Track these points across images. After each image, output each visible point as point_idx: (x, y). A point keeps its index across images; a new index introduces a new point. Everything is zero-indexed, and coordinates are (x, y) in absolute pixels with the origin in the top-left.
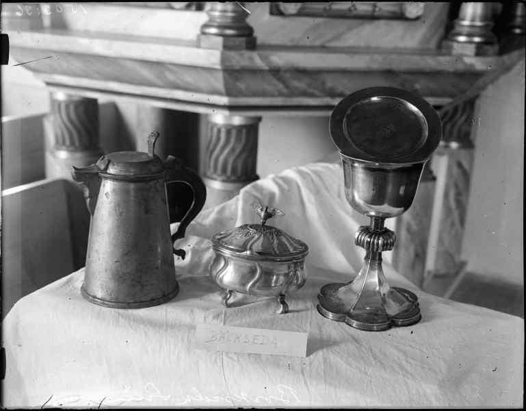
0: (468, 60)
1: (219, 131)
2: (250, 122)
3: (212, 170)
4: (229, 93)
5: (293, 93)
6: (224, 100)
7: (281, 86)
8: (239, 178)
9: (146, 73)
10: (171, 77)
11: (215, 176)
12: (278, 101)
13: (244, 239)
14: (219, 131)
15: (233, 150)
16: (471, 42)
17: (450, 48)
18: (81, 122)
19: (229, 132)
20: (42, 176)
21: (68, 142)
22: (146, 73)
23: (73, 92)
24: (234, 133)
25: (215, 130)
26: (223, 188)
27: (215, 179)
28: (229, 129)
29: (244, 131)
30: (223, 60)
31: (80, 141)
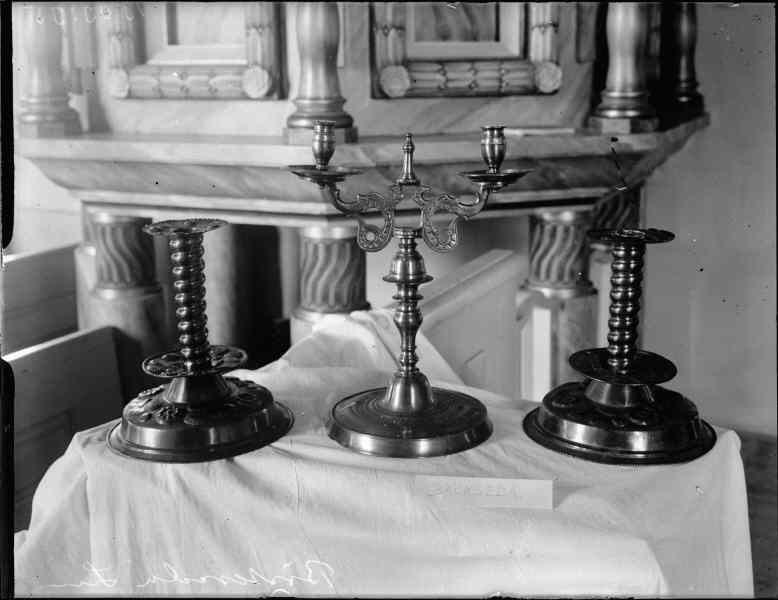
1: (316, 248)
3: (309, 298)
10: (250, 183)
11: (312, 307)
14: (316, 248)
15: (335, 271)
19: (328, 249)
20: (75, 328)
22: (221, 182)
24: (335, 249)
27: (313, 311)
31: (133, 275)
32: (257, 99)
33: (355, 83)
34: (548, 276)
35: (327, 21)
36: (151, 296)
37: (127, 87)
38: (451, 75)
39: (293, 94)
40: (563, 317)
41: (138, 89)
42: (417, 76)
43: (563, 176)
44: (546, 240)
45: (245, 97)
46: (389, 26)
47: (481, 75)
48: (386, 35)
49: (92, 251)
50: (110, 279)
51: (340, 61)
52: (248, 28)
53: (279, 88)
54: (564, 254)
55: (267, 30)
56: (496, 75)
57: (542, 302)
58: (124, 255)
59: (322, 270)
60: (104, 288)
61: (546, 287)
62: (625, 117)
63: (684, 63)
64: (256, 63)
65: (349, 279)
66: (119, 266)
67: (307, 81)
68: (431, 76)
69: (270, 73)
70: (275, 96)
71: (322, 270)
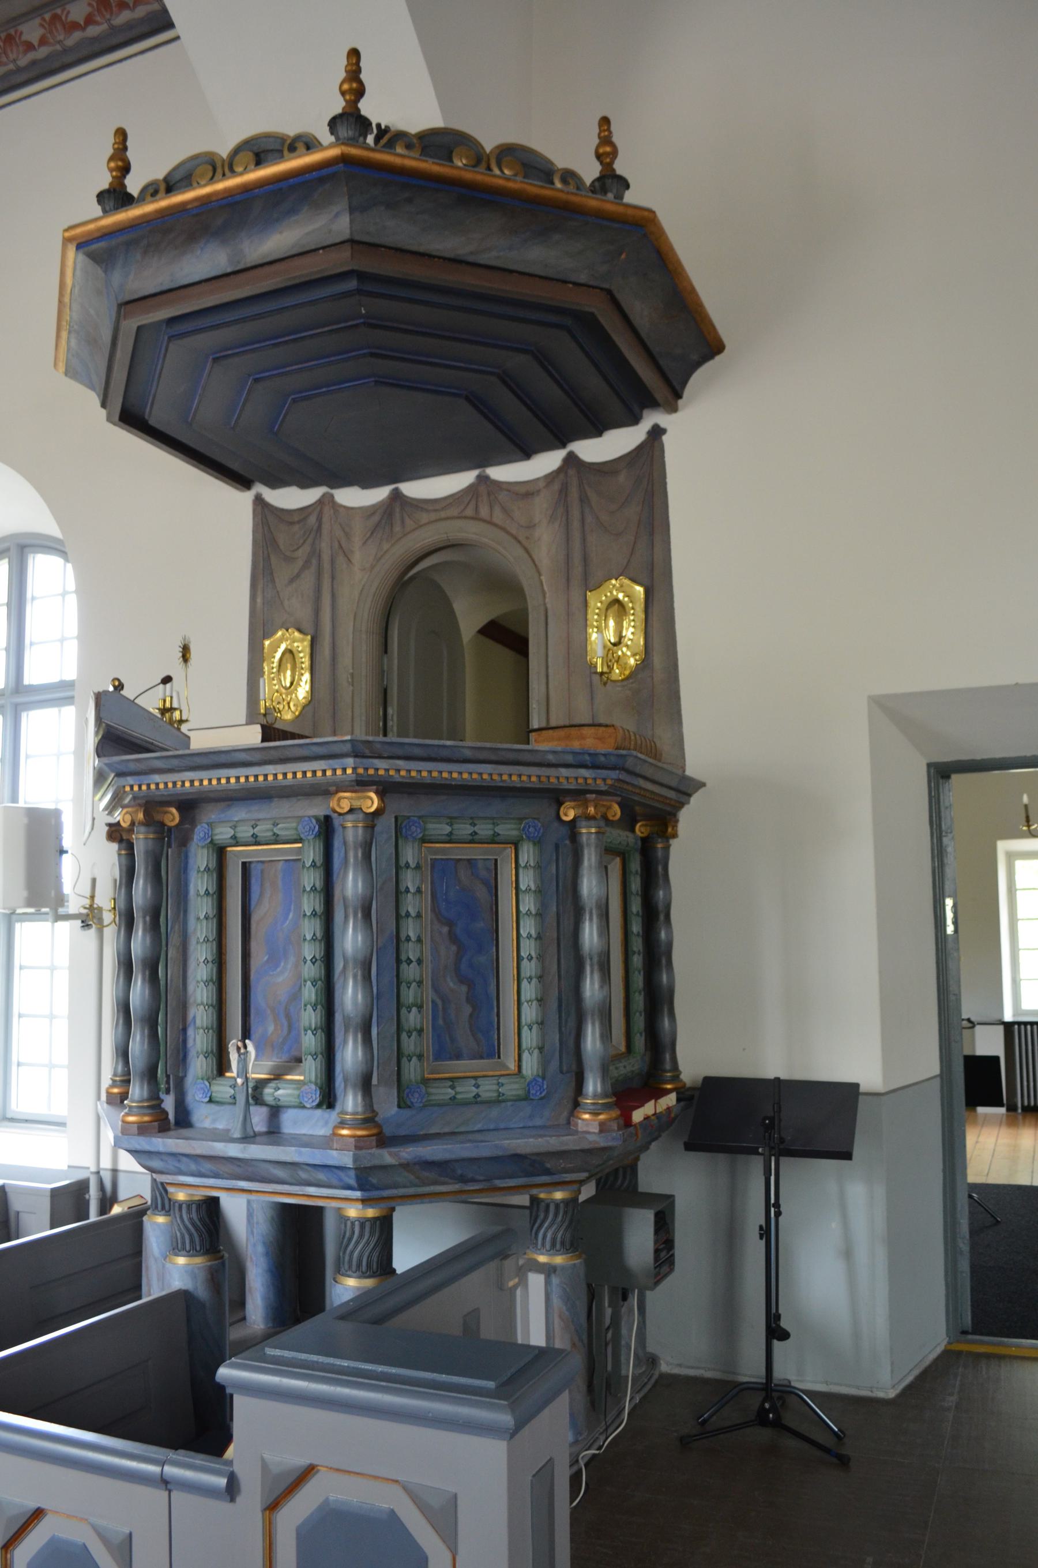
0: (591, 1138)
1: (353, 1224)
2: (384, 1213)
3: (346, 1266)
4: (361, 1187)
7: (412, 1177)
8: (374, 1273)
9: (280, 1173)
10: (303, 1175)
12: (411, 1191)
13: (197, 1025)
14: (353, 1224)
15: (368, 1243)
17: (576, 1125)
18: (204, 1224)
19: (362, 1225)
20: (135, 1290)
22: (280, 1173)
23: (191, 1191)
24: (368, 1225)
25: (349, 1223)
26: (187, 1263)
27: (349, 1276)
28: (363, 1222)
29: (378, 1222)
30: (356, 1159)
31: (202, 1241)
32: (309, 1108)
34: (543, 1245)
35: (365, 1053)
36: (216, 1262)
37: (209, 1095)
39: (338, 1108)
40: (555, 1280)
41: (217, 1096)
42: (431, 1090)
43: (548, 1165)
44: (542, 1216)
45: (304, 1107)
46: (411, 1055)
49: (161, 1219)
50: (184, 1249)
51: (375, 1081)
52: (67, 241)
53: (328, 1099)
54: (554, 1227)
55: (320, 1056)
56: (495, 1087)
57: (540, 1268)
58: (193, 1224)
59: (357, 1243)
61: (542, 1254)
62: (594, 1120)
63: (668, 1056)
64: (310, 1082)
65: (378, 1249)
66: (191, 1235)
67: (350, 1102)
68: (443, 1091)
69: (321, 1088)
70: (325, 1107)
71: (357, 1243)
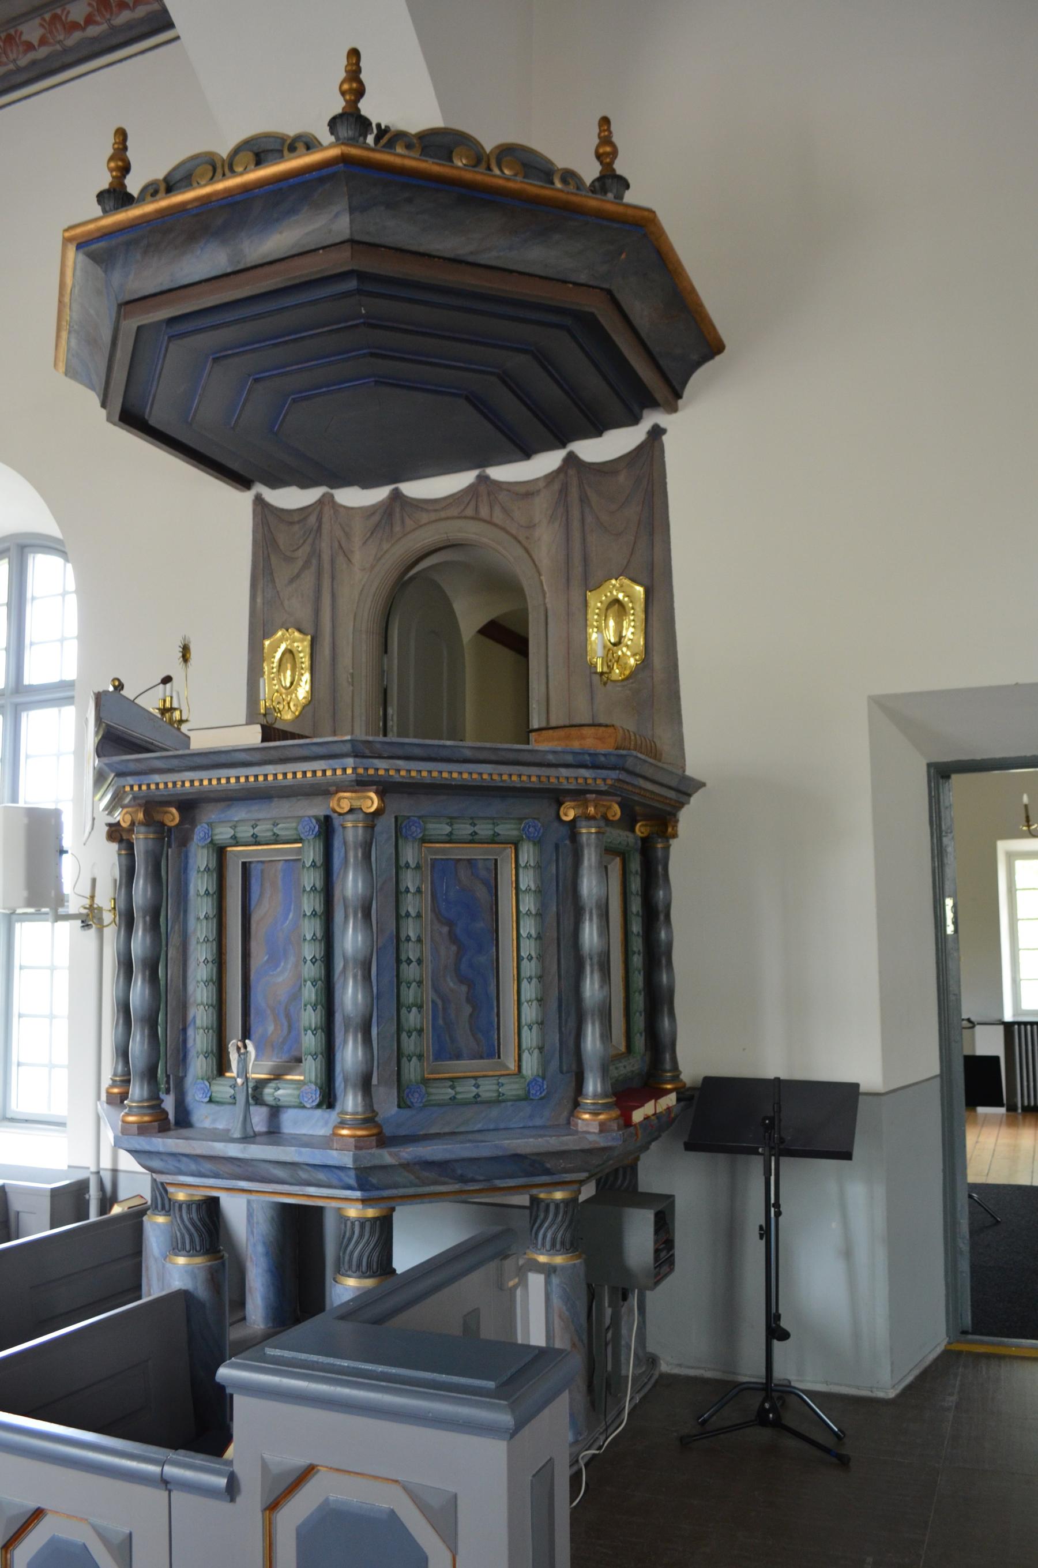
0: (591, 1138)
1: (353, 1224)
2: (384, 1213)
3: (346, 1266)
4: (361, 1187)
5: (424, 1184)
6: (358, 1194)
7: (412, 1177)
8: (374, 1272)
9: (280, 1173)
11: (349, 1273)
12: (411, 1191)
14: (353, 1224)
15: (368, 1243)
16: (594, 1120)
17: (576, 1125)
18: (204, 1225)
19: (362, 1225)
20: (135, 1290)
21: (188, 1247)
22: (280, 1173)
24: (368, 1225)
25: (349, 1223)
26: (187, 1263)
27: (349, 1276)
28: (363, 1222)
29: (378, 1223)
30: (356, 1159)
31: (202, 1241)
33: (387, 1107)
34: (543, 1245)
35: (365, 1054)
38: (458, 1089)
39: (338, 1108)
40: (555, 1280)
43: (548, 1166)
44: (542, 1216)
45: (304, 1107)
46: (411, 1055)
47: (481, 1088)
48: (409, 1061)
49: (161, 1219)
50: (184, 1248)
51: (375, 1081)
53: (328, 1099)
55: (320, 1056)
56: (495, 1087)
57: (540, 1268)
58: (194, 1224)
59: (357, 1243)
60: (177, 1255)
61: (542, 1254)
63: (668, 1056)
64: (311, 1082)
67: (350, 1102)
68: (443, 1091)
69: (321, 1088)
70: (325, 1107)
71: (357, 1243)
